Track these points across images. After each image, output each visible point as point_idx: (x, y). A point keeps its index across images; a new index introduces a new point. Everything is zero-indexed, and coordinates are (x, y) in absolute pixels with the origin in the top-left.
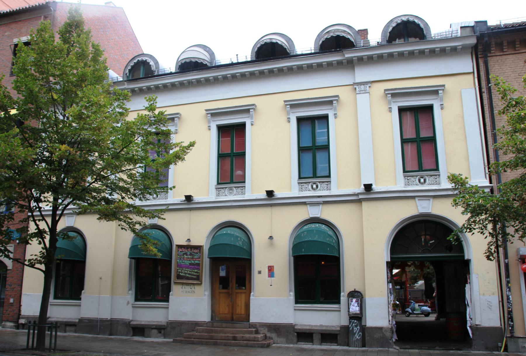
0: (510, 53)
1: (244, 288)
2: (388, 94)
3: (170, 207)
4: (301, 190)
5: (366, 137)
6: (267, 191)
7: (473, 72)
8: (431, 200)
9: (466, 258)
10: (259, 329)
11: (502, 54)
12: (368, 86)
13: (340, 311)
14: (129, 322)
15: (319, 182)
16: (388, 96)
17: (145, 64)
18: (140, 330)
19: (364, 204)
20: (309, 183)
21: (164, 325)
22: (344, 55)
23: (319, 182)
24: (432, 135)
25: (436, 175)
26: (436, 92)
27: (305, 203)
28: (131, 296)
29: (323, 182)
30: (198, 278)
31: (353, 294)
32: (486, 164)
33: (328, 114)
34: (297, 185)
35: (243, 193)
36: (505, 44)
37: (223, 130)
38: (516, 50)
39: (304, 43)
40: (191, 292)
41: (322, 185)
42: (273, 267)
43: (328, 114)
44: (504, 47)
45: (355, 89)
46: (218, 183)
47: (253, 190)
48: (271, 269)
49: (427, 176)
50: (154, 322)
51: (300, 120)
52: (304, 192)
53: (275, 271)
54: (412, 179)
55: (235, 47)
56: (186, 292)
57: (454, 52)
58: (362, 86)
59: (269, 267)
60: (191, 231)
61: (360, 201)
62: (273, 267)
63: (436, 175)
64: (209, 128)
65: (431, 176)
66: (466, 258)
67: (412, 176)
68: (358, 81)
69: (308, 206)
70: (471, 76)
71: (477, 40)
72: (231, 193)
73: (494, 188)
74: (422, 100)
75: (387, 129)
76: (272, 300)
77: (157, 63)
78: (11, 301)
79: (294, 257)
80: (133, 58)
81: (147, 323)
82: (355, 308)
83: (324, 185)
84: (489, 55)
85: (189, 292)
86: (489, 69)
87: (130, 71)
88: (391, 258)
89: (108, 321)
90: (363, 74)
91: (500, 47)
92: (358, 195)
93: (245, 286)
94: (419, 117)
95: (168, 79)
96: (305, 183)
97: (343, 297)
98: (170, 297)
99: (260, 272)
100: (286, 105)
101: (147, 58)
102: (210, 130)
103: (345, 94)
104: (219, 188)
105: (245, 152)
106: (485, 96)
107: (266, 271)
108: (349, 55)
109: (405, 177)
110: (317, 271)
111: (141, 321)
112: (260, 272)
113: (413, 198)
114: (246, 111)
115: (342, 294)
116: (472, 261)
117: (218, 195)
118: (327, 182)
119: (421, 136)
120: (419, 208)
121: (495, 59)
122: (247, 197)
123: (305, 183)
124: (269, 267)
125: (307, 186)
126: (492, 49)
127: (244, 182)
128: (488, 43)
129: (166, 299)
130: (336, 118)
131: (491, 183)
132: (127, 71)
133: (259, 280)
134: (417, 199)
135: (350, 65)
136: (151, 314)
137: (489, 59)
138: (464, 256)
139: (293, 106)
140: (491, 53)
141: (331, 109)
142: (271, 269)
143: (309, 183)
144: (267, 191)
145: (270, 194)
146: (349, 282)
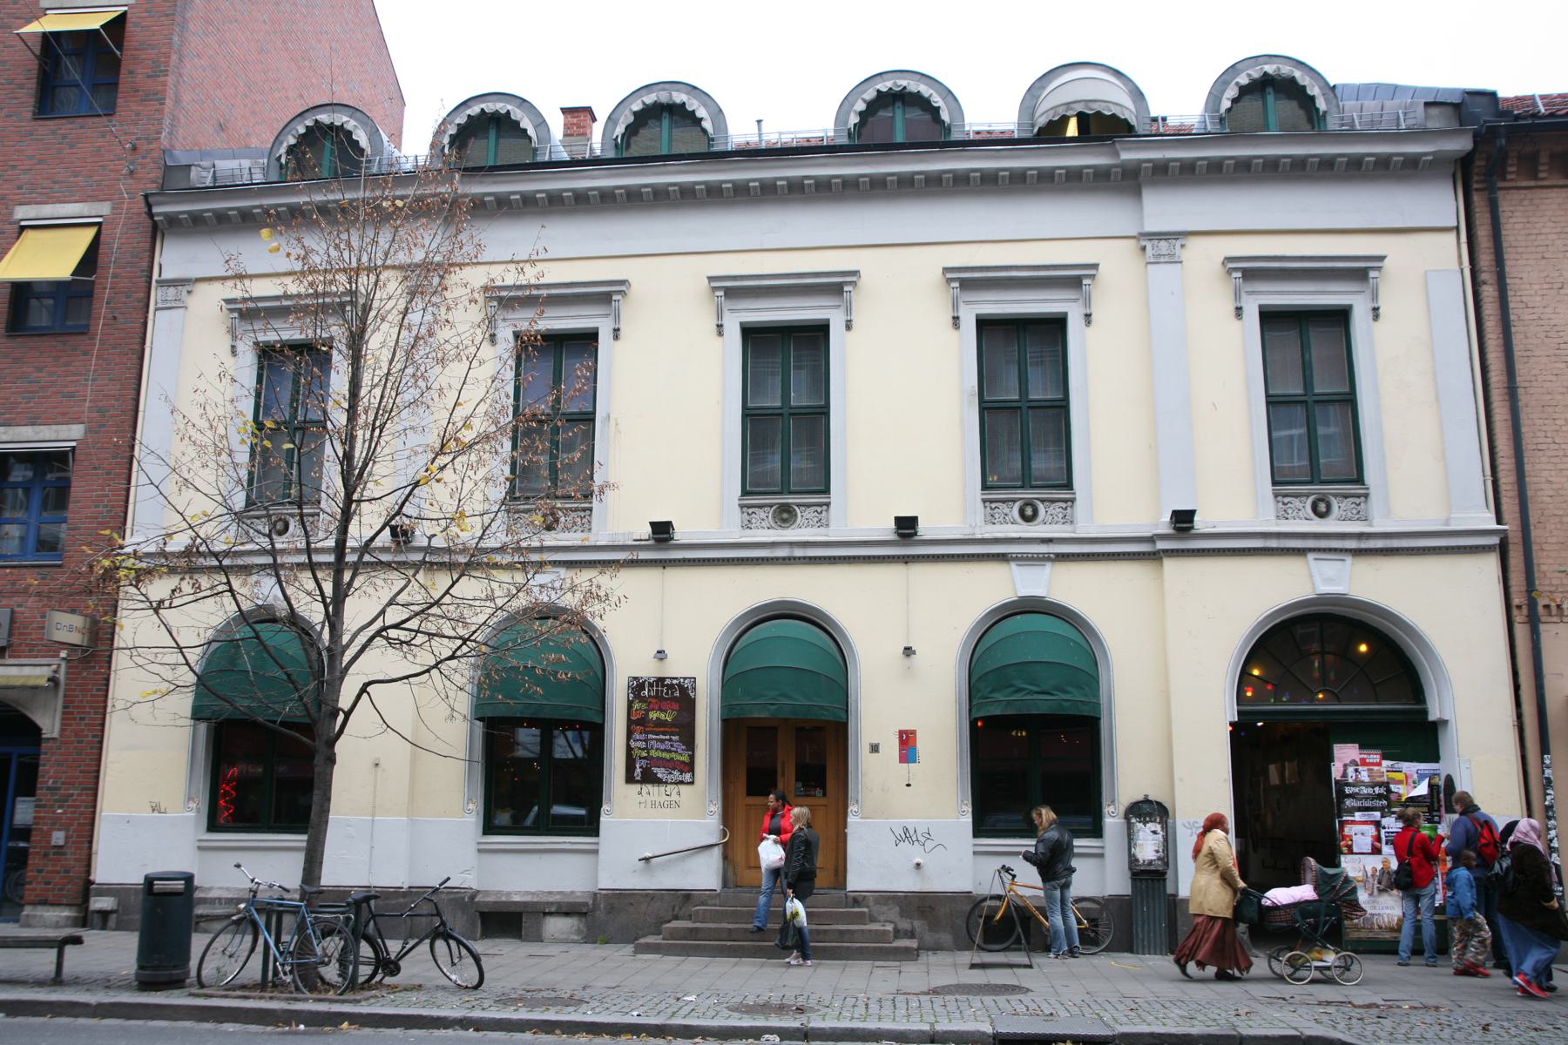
0: (1554, 182)
1: (819, 792)
2: (1236, 269)
3: (798, 553)
4: (991, 520)
5: (1167, 385)
6: (652, 524)
7: (1458, 228)
8: (1349, 559)
9: (1432, 717)
10: (875, 908)
11: (1532, 183)
12: (1178, 243)
13: (1101, 856)
14: (473, 897)
15: (1043, 501)
16: (1235, 275)
17: (678, 114)
18: (507, 921)
19: (1168, 564)
20: (1014, 501)
21: (586, 904)
22: (1117, 154)
23: (1043, 501)
24: (1347, 390)
25: (1358, 496)
26: (1074, 283)
27: (1003, 558)
28: (471, 818)
29: (1053, 501)
30: (690, 767)
31: (1149, 810)
32: (1488, 472)
33: (1066, 314)
34: (980, 505)
35: (823, 524)
36: (1544, 158)
37: (760, 341)
38: (1536, 178)
39: (989, 104)
40: (670, 806)
41: (1051, 510)
42: (914, 732)
43: (1066, 314)
44: (1510, 169)
45: (1144, 248)
46: (745, 493)
47: (621, 516)
48: (907, 740)
49: (1335, 496)
50: (550, 893)
51: (753, 335)
52: (997, 527)
53: (919, 745)
54: (1296, 502)
55: (782, 96)
56: (653, 804)
57: (1408, 170)
58: (1163, 243)
59: (901, 733)
60: (665, 631)
61: (1156, 556)
62: (914, 732)
63: (1358, 496)
64: (1239, 311)
65: (1346, 497)
66: (1432, 717)
67: (1296, 496)
68: (1151, 227)
69: (1013, 565)
70: (1453, 235)
71: (1475, 142)
72: (784, 521)
73: (1510, 535)
74: (997, 302)
75: (1226, 366)
76: (911, 822)
77: (718, 114)
78: (58, 837)
79: (724, 721)
80: (465, 104)
81: (528, 899)
82: (1148, 847)
83: (1056, 509)
84: (1500, 184)
85: (662, 806)
86: (1502, 220)
87: (453, 139)
88: (1239, 713)
89: (405, 894)
90: (1165, 209)
91: (1530, 168)
92: (1151, 540)
93: (823, 786)
94: (1312, 340)
95: (593, 178)
96: (1003, 501)
97: (1112, 821)
98: (603, 819)
99: (875, 748)
100: (715, 289)
101: (509, 107)
102: (720, 334)
103: (1116, 265)
104: (749, 506)
105: (827, 405)
106: (1489, 292)
107: (891, 747)
108: (1129, 155)
109: (1276, 496)
110: (1035, 745)
111: (509, 894)
112: (875, 748)
113: (1301, 552)
114: (836, 287)
115: (1107, 810)
116: (1452, 726)
117: (747, 526)
118: (1065, 501)
119: (1031, 397)
120: (1318, 581)
121: (1516, 196)
122: (599, 536)
123: (1003, 501)
124: (901, 733)
125: (1007, 510)
126: (1510, 169)
127: (827, 491)
128: (1502, 151)
129: (589, 826)
130: (616, 337)
131: (1499, 522)
132: (446, 140)
133: (873, 771)
134: (1311, 556)
135: (1129, 182)
136: (534, 870)
137: (1500, 194)
138: (1425, 712)
139: (731, 293)
140: (1504, 180)
141: (607, 315)
142: (907, 740)
143: (1014, 501)
144: (652, 524)
145: (662, 531)
146: (1129, 773)
